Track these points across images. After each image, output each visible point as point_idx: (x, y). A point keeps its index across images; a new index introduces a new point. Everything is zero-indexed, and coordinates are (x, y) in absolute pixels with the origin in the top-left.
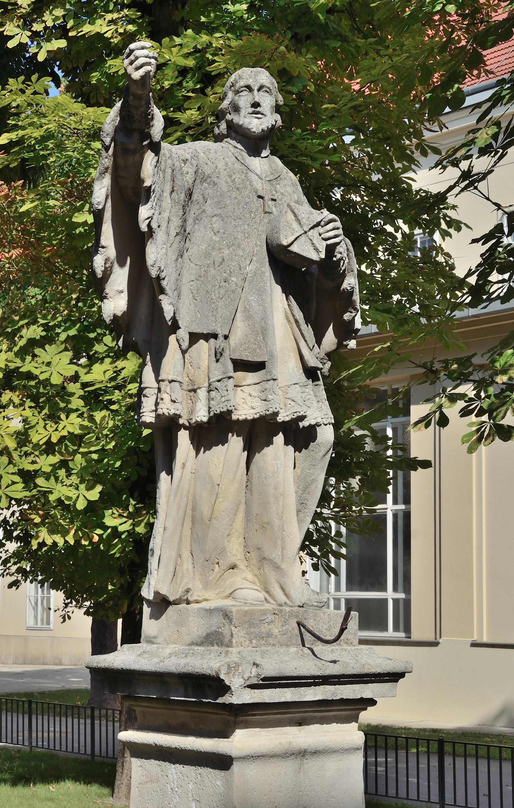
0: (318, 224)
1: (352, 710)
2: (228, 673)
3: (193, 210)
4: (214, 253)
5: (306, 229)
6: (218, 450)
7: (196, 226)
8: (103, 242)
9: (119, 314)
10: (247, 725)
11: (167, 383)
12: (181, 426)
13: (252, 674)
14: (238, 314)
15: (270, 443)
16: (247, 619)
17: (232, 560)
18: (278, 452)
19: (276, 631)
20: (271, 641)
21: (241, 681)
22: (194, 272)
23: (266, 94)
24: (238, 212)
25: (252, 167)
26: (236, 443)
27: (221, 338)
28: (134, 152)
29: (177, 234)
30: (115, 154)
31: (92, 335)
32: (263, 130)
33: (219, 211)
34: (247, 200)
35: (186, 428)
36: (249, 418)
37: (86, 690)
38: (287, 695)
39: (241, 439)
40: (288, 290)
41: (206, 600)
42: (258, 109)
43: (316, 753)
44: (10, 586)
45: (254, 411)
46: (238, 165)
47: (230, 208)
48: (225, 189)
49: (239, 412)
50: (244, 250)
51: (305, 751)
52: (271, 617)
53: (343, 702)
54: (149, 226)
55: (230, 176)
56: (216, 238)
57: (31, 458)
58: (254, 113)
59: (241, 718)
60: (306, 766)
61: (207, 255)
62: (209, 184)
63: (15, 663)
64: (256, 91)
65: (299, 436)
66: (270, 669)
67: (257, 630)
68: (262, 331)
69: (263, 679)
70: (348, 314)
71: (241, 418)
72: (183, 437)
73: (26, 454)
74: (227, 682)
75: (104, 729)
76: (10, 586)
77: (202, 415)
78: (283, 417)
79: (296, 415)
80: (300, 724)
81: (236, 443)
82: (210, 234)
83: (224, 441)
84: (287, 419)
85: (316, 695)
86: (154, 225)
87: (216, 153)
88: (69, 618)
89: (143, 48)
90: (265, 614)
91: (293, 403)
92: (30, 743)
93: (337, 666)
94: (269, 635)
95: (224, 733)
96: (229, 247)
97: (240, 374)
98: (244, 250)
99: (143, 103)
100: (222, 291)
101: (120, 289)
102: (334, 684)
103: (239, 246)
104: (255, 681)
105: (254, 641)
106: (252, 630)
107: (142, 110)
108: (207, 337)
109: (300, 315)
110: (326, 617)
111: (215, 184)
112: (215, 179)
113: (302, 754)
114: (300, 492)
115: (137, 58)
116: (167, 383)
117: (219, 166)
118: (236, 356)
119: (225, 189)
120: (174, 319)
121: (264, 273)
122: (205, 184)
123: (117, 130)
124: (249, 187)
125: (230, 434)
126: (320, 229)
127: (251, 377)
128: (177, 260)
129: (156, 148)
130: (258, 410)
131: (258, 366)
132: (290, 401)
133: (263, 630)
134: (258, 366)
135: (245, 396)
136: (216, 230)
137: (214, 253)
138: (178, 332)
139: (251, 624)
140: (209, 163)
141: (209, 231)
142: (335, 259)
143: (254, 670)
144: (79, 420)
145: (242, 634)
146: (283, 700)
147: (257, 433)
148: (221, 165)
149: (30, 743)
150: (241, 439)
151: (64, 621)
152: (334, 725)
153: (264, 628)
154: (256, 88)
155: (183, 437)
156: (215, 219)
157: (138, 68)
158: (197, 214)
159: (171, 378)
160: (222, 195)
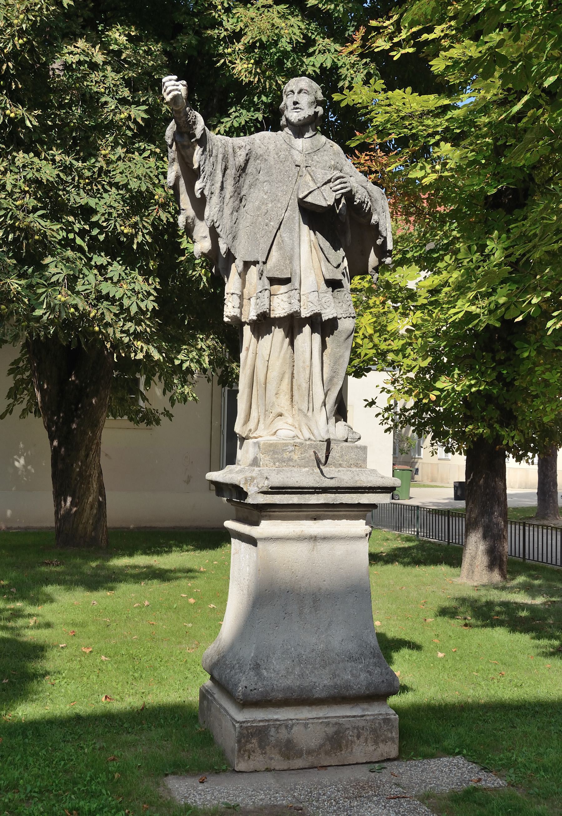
0: (329, 181)
1: (357, 511)
2: (245, 484)
3: (248, 180)
4: (263, 207)
5: (319, 185)
6: (267, 337)
7: (252, 190)
8: (182, 207)
9: (206, 252)
10: (270, 518)
11: (230, 295)
12: (243, 324)
13: (265, 484)
14: (274, 247)
15: (300, 331)
16: (272, 449)
17: (279, 410)
18: (307, 339)
19: (296, 457)
20: (291, 464)
21: (256, 489)
22: (249, 220)
23: (305, 95)
24: (279, 178)
25: (296, 146)
26: (278, 333)
27: (261, 263)
28: (188, 147)
29: (231, 197)
30: (178, 149)
31: (435, 255)
32: (299, 120)
33: (268, 178)
34: (287, 169)
35: (248, 324)
36: (282, 316)
37: (535, 507)
38: (295, 499)
39: (282, 330)
40: (313, 227)
41: (261, 437)
42: (297, 106)
43: (325, 538)
44: (386, 431)
45: (284, 311)
46: (285, 146)
47: (275, 176)
48: (272, 163)
49: (275, 312)
50: (282, 203)
51: (316, 537)
52: (291, 448)
53: (359, 505)
54: (202, 193)
55: (277, 154)
56: (265, 197)
57: (387, 343)
58: (294, 109)
59: (265, 513)
60: (319, 547)
61: (259, 208)
62: (261, 161)
63: (519, 488)
64: (296, 93)
65: (324, 327)
66: (277, 480)
67: (280, 457)
68: (290, 258)
69: (271, 488)
70: (379, 240)
71: (277, 316)
72: (247, 330)
73: (386, 340)
74: (245, 490)
75: (531, 533)
76: (386, 431)
77: (253, 316)
78: (305, 313)
79: (313, 313)
80: (315, 519)
81: (278, 333)
82: (262, 194)
83: (269, 332)
84: (308, 315)
85: (318, 500)
86: (206, 193)
87: (269, 139)
88: (436, 453)
89: (170, 80)
90: (287, 446)
91: (311, 305)
92: (449, 540)
93: (333, 480)
94: (290, 459)
95: (256, 523)
96: (272, 201)
97: (276, 287)
98: (282, 203)
99: (182, 115)
100: (263, 232)
101: (204, 235)
102: (335, 493)
103: (279, 201)
104: (265, 489)
105: (277, 464)
106: (276, 456)
107: (183, 119)
108: (255, 263)
109: (326, 245)
110: (339, 448)
111: (266, 160)
112: (266, 157)
113: (314, 539)
114: (332, 364)
115: (167, 87)
116: (230, 295)
117: (270, 148)
118: (270, 275)
119: (272, 163)
120: (229, 252)
121: (294, 217)
122: (258, 161)
123: (175, 134)
124: (290, 159)
125: (273, 327)
126: (331, 184)
127: (283, 289)
128: (232, 213)
129: (203, 141)
130: (286, 310)
131: (286, 281)
132: (310, 303)
133: (285, 456)
134: (286, 281)
135: (279, 301)
136: (266, 191)
137: (263, 207)
138: (236, 261)
139: (275, 452)
140: (262, 146)
141: (262, 192)
142: (355, 203)
143: (266, 482)
144: (422, 314)
145: (267, 458)
146: (290, 502)
147: (292, 325)
148: (271, 147)
149: (449, 540)
150: (282, 330)
151: (433, 455)
152: (344, 521)
153: (286, 455)
154: (296, 92)
155: (247, 330)
156: (265, 184)
157: (168, 94)
158: (251, 181)
159: (232, 291)
160: (270, 167)
